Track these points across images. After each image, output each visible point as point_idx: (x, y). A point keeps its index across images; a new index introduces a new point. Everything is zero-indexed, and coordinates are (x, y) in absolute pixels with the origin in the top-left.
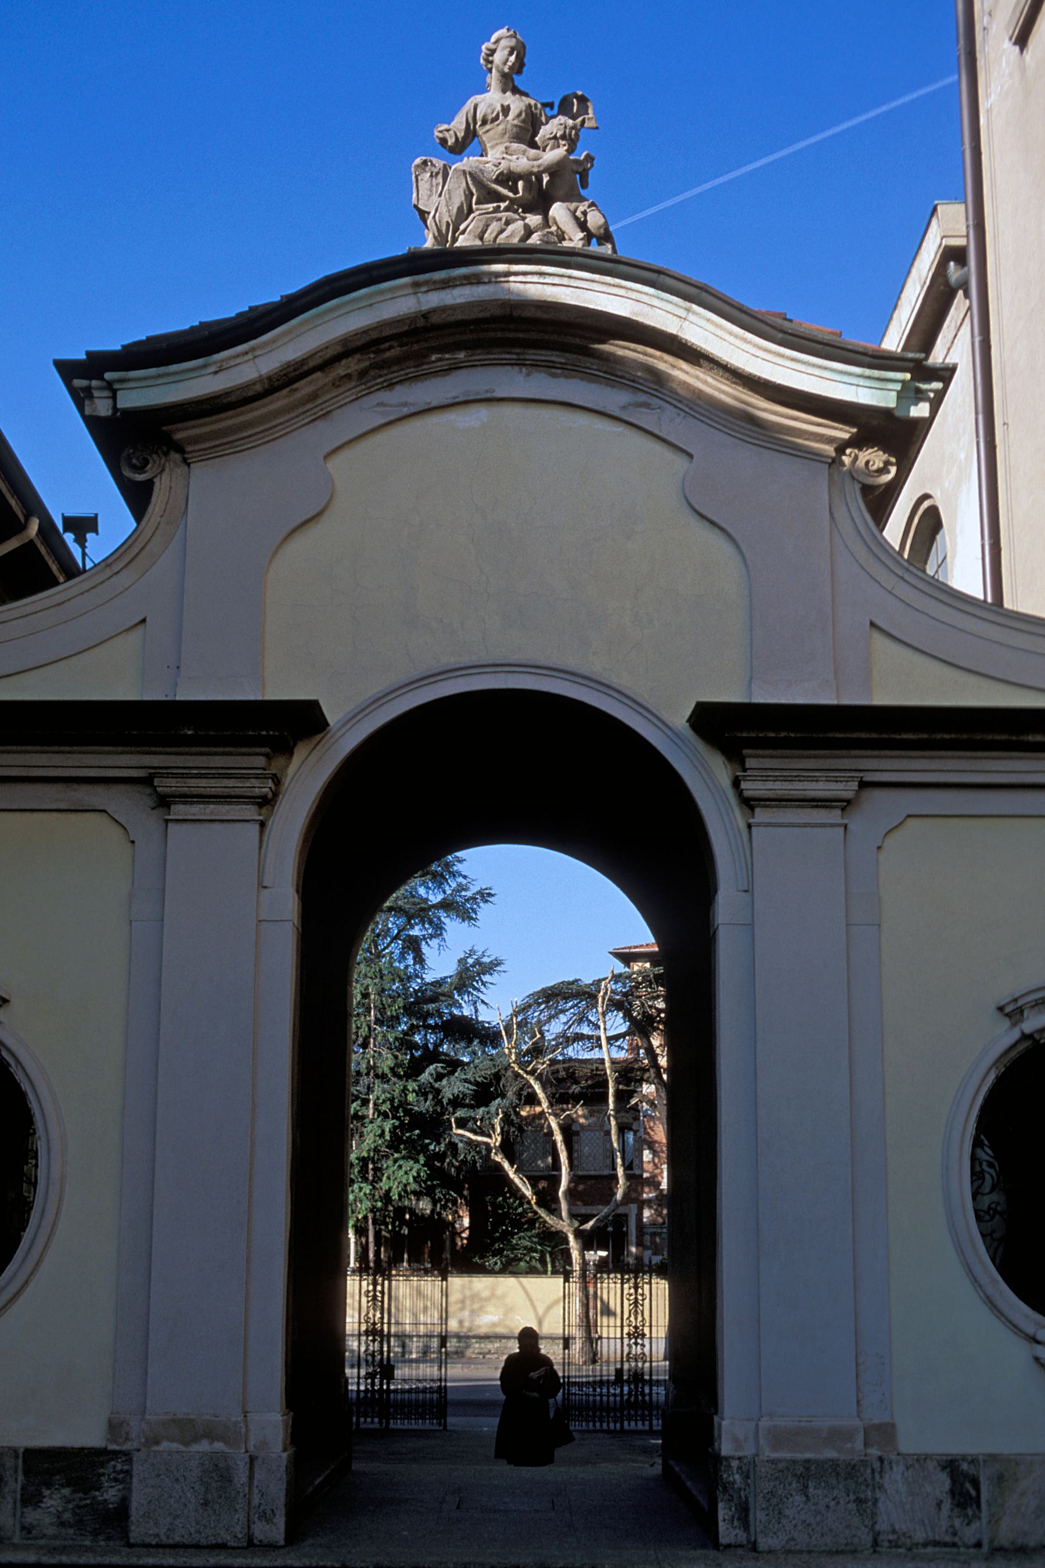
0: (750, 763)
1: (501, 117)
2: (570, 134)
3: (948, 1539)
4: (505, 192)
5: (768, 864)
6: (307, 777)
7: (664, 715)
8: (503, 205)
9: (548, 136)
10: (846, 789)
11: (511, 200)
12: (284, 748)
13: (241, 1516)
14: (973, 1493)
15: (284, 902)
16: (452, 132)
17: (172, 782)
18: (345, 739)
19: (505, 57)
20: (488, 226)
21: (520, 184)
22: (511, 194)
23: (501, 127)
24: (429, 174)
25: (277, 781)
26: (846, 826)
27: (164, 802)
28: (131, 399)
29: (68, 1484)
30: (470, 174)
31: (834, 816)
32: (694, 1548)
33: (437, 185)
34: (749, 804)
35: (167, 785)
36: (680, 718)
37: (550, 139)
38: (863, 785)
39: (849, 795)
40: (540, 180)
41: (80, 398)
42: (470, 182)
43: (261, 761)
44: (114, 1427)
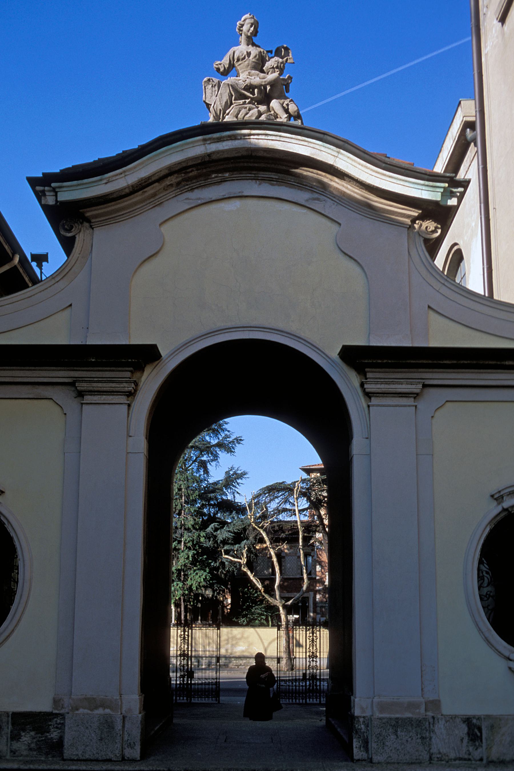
0: (369, 375)
1: (246, 58)
2: (280, 66)
3: (466, 757)
4: (248, 94)
5: (378, 425)
6: (151, 382)
7: (327, 352)
8: (247, 101)
9: (269, 67)
10: (416, 388)
11: (251, 98)
12: (140, 368)
13: (119, 745)
14: (479, 734)
15: (140, 443)
16: (222, 65)
17: (85, 385)
18: (170, 363)
19: (249, 28)
20: (240, 111)
21: (256, 90)
22: (251, 96)
23: (246, 63)
24: (211, 86)
25: (136, 384)
26: (416, 406)
27: (81, 394)
29: (33, 730)
30: (231, 85)
31: (410, 401)
32: (342, 761)
33: (215, 91)
34: (368, 395)
35: (82, 386)
36: (334, 353)
37: (270, 68)
38: (425, 386)
39: (418, 391)
40: (265, 88)
42: (231, 90)
43: (128, 374)
44: (56, 702)
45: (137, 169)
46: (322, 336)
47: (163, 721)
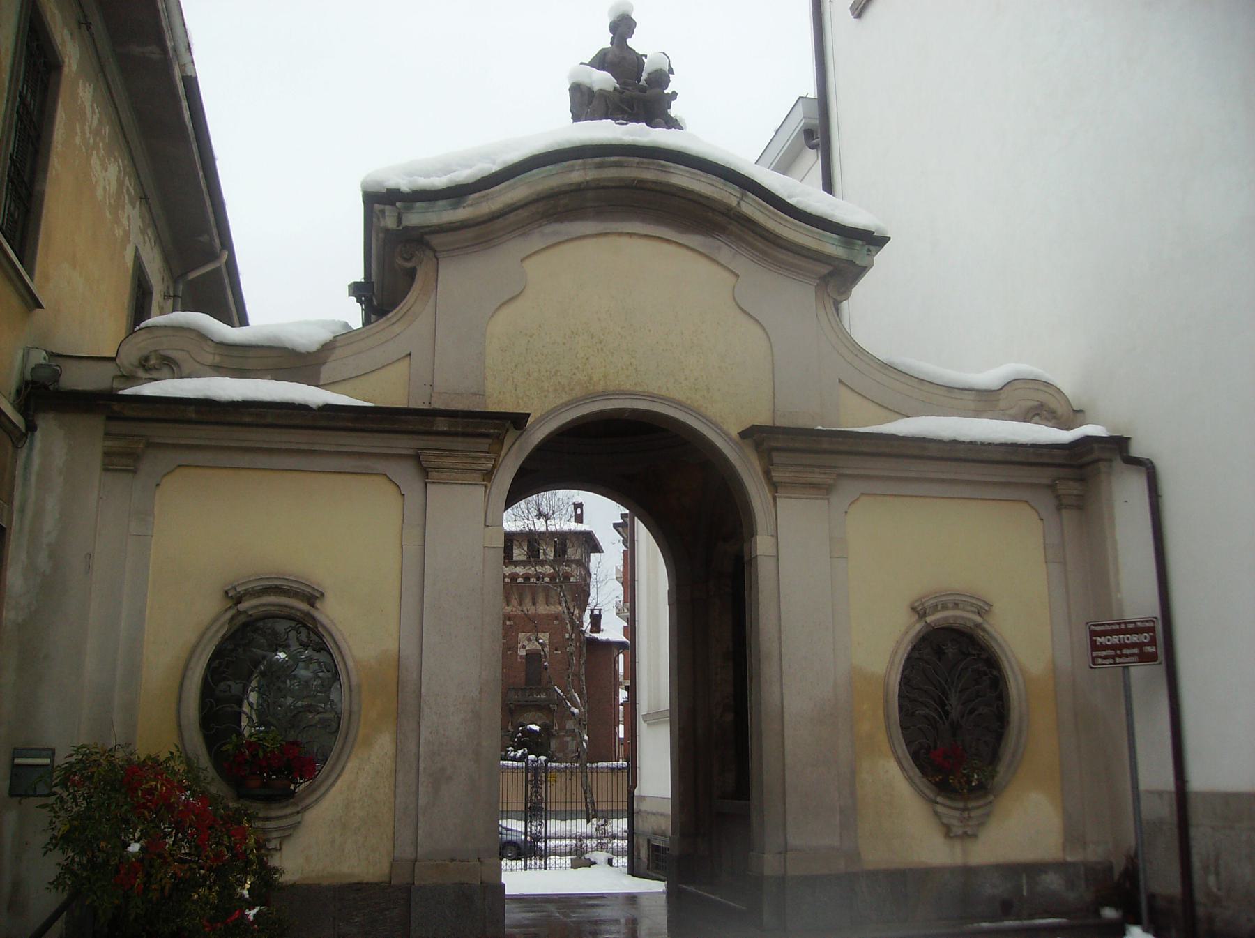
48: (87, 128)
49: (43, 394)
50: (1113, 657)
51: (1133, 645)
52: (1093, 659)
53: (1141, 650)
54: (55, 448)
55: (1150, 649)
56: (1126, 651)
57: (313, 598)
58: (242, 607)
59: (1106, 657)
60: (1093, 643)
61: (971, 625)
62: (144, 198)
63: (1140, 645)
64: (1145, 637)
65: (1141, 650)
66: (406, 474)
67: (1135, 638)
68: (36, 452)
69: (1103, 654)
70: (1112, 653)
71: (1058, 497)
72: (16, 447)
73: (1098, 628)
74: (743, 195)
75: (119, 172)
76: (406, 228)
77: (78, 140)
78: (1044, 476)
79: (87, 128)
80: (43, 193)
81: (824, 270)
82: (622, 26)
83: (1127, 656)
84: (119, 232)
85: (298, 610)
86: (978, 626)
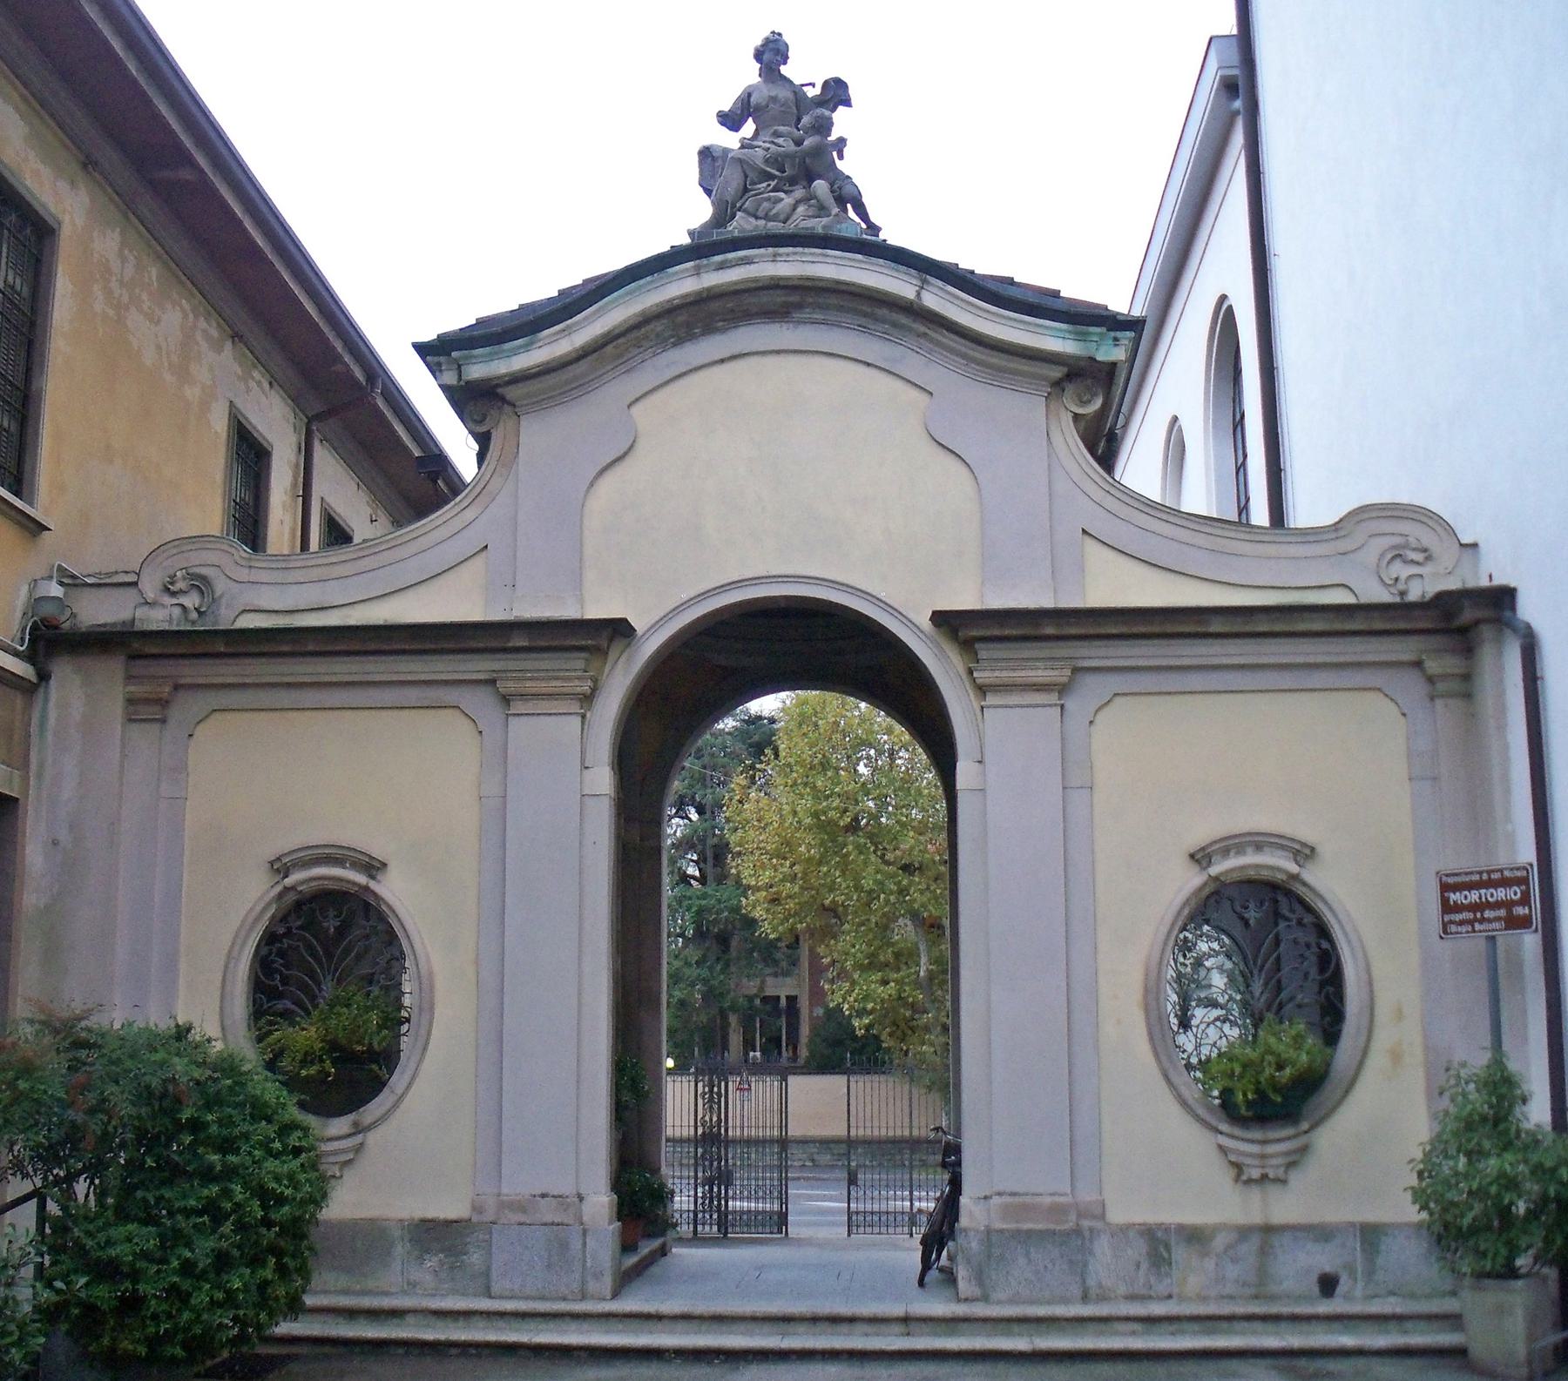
0: (983, 654)
3: (1144, 1291)
5: (1000, 740)
6: (620, 679)
7: (911, 616)
8: (773, 184)
10: (1060, 675)
11: (780, 179)
12: (600, 652)
13: (577, 1276)
14: (1165, 1255)
15: (603, 780)
17: (510, 684)
18: (649, 647)
25: (595, 681)
26: (1062, 706)
27: (506, 700)
28: (477, 371)
29: (442, 1251)
31: (1053, 698)
34: (982, 690)
35: (506, 686)
36: (924, 621)
38: (1076, 670)
39: (1065, 679)
41: (434, 370)
43: (580, 664)
44: (477, 1208)
45: (243, 933)
46: (904, 584)
47: (728, 724)
48: (114, 285)
49: (50, 640)
50: (1471, 922)
51: (1498, 905)
52: (1445, 925)
53: (1510, 911)
54: (78, 696)
55: (1521, 911)
56: (1487, 914)
57: (373, 867)
58: (288, 881)
59: (1461, 923)
60: (1445, 902)
61: (1280, 876)
62: (236, 337)
63: (1508, 905)
64: (1514, 893)
65: (1510, 911)
66: (481, 703)
67: (1501, 894)
68: (51, 704)
69: (1458, 917)
70: (1470, 916)
71: (1431, 680)
72: (29, 706)
73: (1451, 880)
74: (924, 281)
75: (185, 316)
76: (467, 383)
77: (98, 307)
78: (1403, 650)
79: (114, 285)
80: (40, 391)
81: (1057, 373)
82: (772, 53)
83: (1489, 921)
84: (192, 393)
85: (354, 883)
86: (1295, 877)
